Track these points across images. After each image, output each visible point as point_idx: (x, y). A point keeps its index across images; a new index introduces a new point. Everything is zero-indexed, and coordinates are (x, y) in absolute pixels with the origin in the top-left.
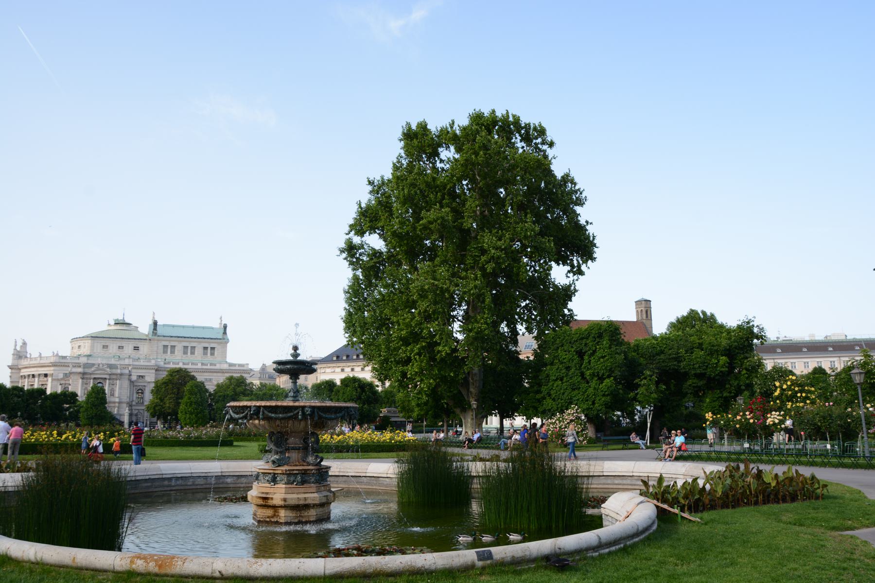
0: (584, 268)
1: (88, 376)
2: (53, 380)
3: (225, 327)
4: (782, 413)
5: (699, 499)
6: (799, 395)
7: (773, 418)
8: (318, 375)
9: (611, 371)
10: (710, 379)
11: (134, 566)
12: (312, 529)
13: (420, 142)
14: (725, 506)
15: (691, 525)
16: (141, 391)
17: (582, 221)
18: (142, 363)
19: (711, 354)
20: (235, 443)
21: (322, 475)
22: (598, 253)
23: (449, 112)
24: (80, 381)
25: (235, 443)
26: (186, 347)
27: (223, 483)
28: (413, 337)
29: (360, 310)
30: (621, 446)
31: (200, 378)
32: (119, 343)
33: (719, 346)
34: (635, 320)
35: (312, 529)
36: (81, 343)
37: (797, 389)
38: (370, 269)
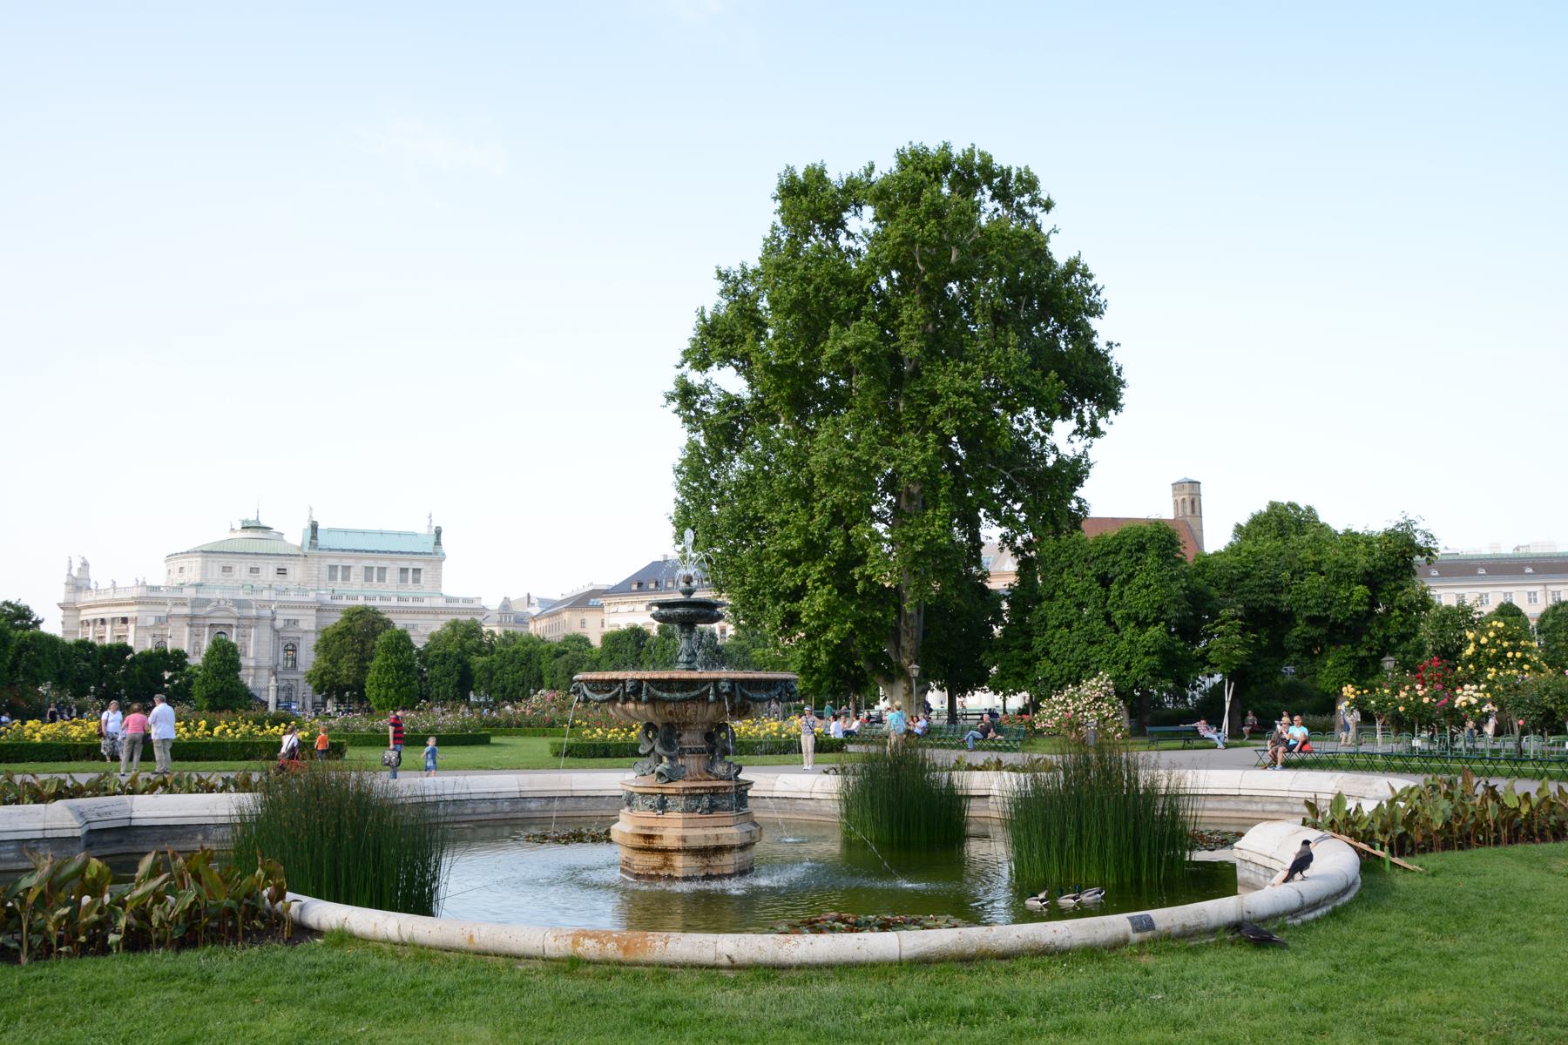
0: (1101, 423)
1: (201, 622)
2: (136, 628)
3: (438, 533)
4: (1483, 686)
5: (1405, 834)
6: (1510, 655)
7: (1467, 695)
8: (605, 617)
9: (1161, 610)
10: (1335, 627)
11: (579, 949)
12: (735, 887)
13: (810, 201)
14: (1447, 845)
15: (1409, 875)
16: (292, 648)
17: (1100, 343)
18: (292, 597)
19: (1338, 581)
20: (493, 740)
21: (741, 795)
22: (1127, 396)
23: (860, 149)
24: (187, 629)
25: (493, 740)
26: (369, 569)
27: (523, 810)
28: (813, 550)
29: (703, 502)
30: (1180, 744)
31: (400, 623)
32: (225, 561)
33: (1353, 566)
34: (1172, 517)
35: (735, 887)
36: (184, 563)
37: (1505, 644)
38: (723, 430)
